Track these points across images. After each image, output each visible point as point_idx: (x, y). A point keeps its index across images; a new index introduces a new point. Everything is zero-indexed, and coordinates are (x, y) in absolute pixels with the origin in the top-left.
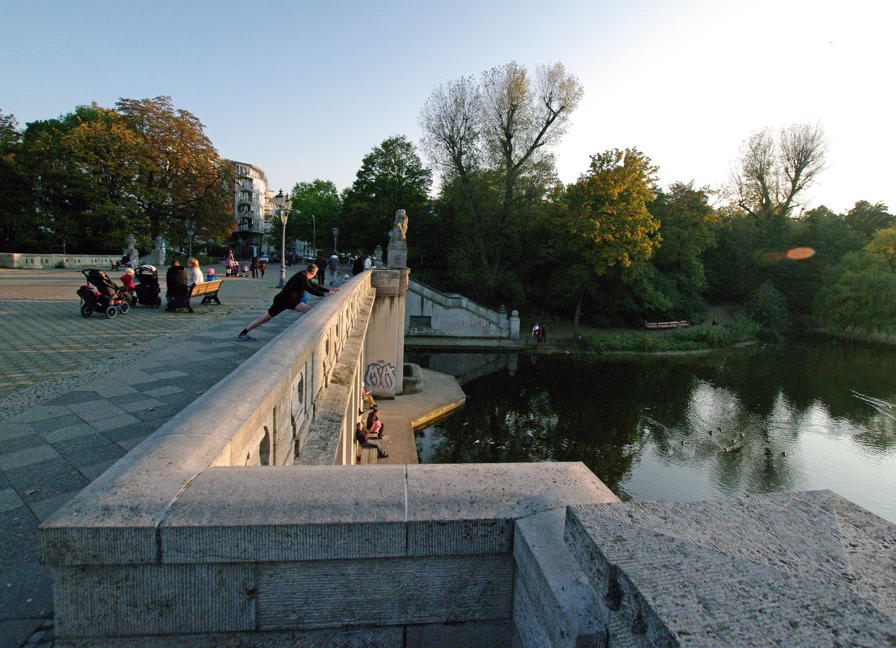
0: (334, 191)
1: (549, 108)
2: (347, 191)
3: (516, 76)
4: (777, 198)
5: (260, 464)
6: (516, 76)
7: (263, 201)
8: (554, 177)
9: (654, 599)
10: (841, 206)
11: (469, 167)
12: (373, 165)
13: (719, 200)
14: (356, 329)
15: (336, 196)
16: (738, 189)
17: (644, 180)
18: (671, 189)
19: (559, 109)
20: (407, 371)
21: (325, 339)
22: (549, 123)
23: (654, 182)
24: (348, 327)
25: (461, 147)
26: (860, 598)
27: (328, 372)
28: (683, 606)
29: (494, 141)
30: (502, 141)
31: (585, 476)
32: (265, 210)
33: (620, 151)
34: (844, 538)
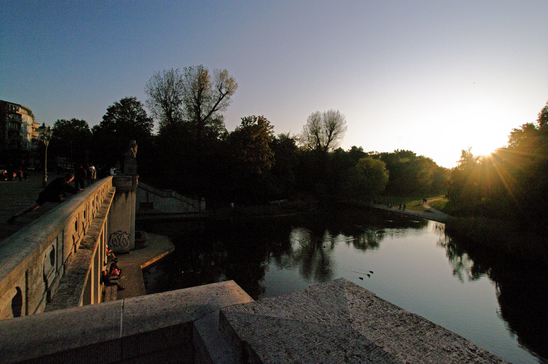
0: (87, 126)
1: (221, 92)
2: (96, 127)
3: (203, 73)
4: (323, 144)
5: (12, 315)
6: (203, 73)
7: (30, 130)
8: (223, 127)
9: (264, 356)
10: (347, 148)
11: (176, 119)
12: (114, 113)
13: (300, 143)
14: (100, 212)
15: (89, 130)
16: (307, 138)
17: (267, 132)
18: (279, 137)
19: (225, 93)
20: (138, 236)
21: (74, 220)
22: (220, 99)
23: (271, 133)
24: (94, 212)
25: (171, 107)
26: (355, 330)
27: (77, 242)
28: (278, 356)
29: (190, 106)
30: (195, 106)
31: (234, 288)
32: (32, 136)
33: (256, 117)
34: (349, 300)
